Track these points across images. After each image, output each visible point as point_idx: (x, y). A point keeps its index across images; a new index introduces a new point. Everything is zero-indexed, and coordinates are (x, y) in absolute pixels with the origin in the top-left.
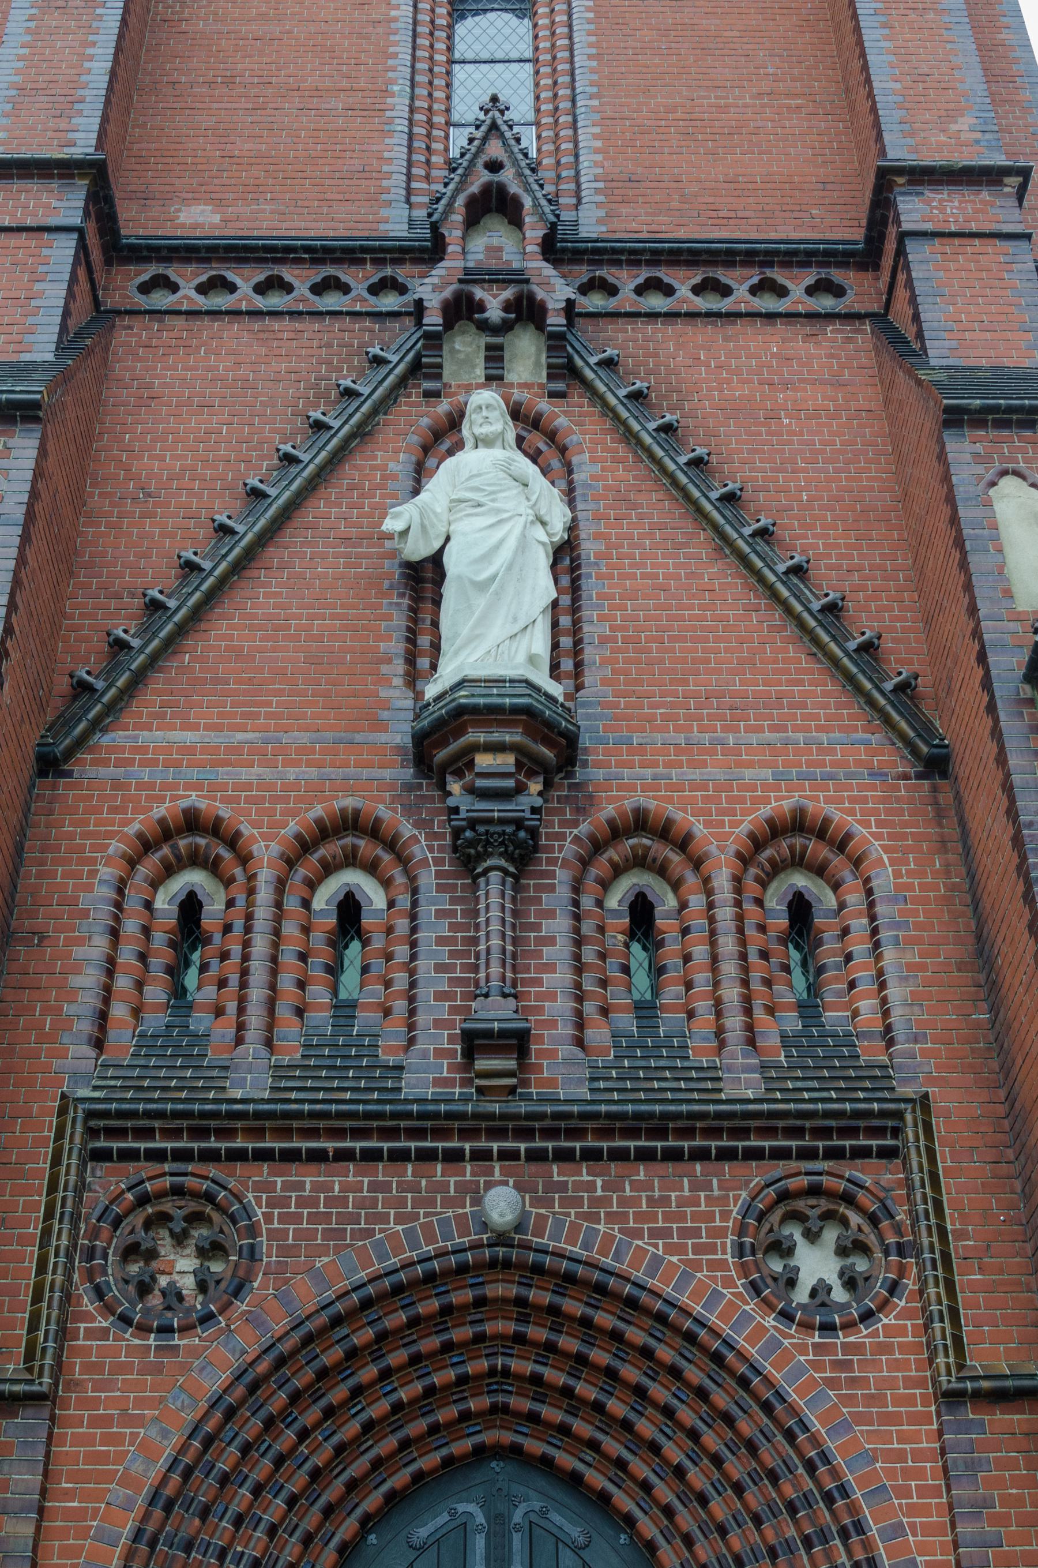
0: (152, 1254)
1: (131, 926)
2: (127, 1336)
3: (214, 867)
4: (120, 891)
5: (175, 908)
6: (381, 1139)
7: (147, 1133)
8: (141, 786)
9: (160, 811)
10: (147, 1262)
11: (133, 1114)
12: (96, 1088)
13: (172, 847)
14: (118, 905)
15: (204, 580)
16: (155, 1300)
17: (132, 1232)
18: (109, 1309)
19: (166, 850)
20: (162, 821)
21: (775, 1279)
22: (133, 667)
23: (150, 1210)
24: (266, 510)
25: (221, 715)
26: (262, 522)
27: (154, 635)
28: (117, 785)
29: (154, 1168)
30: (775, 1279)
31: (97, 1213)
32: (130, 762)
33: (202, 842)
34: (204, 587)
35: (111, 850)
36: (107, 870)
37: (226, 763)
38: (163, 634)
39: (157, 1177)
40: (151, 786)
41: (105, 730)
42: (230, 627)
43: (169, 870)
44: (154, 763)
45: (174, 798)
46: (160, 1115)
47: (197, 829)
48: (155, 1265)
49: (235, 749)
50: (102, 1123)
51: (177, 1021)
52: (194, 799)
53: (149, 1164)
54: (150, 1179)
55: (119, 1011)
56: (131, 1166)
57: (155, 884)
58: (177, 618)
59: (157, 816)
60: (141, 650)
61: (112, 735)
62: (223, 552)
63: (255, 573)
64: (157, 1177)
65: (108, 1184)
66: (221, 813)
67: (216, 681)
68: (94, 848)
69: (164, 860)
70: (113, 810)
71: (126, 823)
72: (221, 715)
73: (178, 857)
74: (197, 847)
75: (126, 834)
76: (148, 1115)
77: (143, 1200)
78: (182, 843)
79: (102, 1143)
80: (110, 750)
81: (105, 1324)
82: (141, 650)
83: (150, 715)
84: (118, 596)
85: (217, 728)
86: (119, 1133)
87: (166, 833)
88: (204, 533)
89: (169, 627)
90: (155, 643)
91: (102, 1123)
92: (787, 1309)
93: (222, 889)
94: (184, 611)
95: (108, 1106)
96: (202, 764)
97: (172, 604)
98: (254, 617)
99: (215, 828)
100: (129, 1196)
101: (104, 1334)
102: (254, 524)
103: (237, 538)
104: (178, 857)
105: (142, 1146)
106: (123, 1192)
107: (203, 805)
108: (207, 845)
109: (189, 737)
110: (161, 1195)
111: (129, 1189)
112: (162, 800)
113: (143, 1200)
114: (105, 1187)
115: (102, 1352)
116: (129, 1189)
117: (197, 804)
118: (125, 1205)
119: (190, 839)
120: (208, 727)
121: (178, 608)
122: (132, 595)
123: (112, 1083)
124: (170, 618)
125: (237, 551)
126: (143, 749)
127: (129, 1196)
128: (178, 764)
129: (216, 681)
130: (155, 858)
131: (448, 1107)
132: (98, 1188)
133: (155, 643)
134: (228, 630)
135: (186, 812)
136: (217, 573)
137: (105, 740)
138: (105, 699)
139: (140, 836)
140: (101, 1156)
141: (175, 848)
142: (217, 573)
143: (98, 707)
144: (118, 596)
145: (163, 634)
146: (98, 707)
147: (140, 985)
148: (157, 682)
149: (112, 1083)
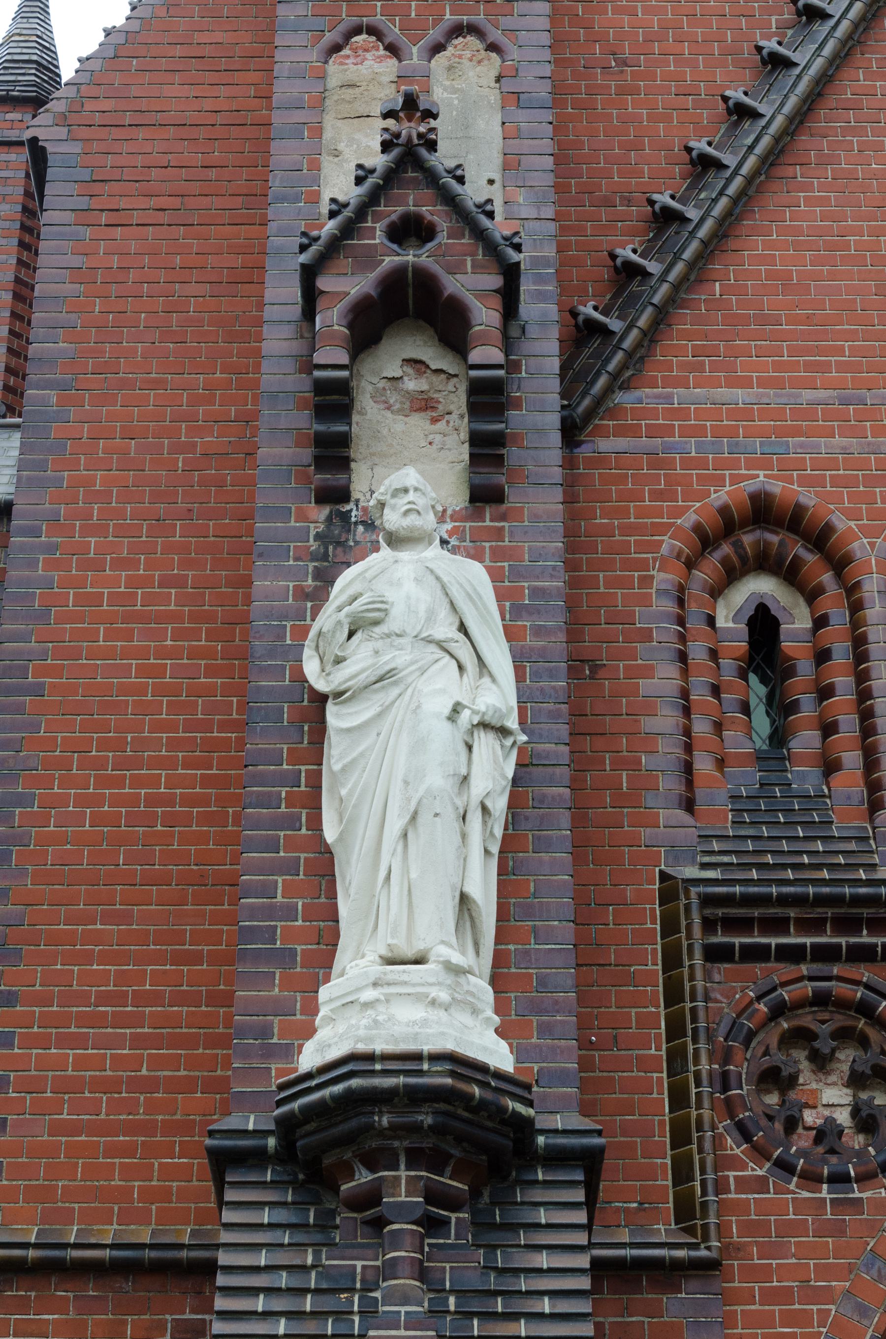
0: (792, 1081)
1: (698, 651)
2: (792, 1187)
3: (791, 574)
4: (681, 602)
5: (743, 627)
6: (764, 932)
7: (779, 925)
8: (688, 463)
9: (720, 496)
10: (783, 1092)
11: (764, 900)
12: (704, 866)
13: (734, 544)
14: (681, 621)
15: (729, 181)
16: (802, 1141)
17: (766, 1053)
18: (760, 1153)
19: (726, 549)
20: (724, 511)
21: (771, 1118)
22: (656, 300)
23: (786, 1025)
24: (795, 85)
25: (778, 366)
26: (792, 101)
27: (677, 257)
28: (656, 461)
29: (787, 970)
30: (771, 1118)
31: (723, 1029)
32: (668, 431)
33: (774, 539)
34: (731, 190)
35: (664, 549)
36: (663, 575)
37: (796, 432)
38: (687, 255)
39: (797, 983)
40: (702, 464)
41: (626, 386)
42: (767, 246)
43: (732, 575)
44: (700, 431)
45: (735, 479)
46: (799, 901)
47: (767, 522)
48: (792, 1095)
49: (805, 413)
50: (720, 912)
51: (773, 777)
52: (761, 480)
53: (782, 965)
54: (784, 984)
55: (703, 764)
56: (758, 968)
57: (716, 592)
58: (702, 233)
59: (718, 504)
60: (662, 279)
61: (638, 393)
62: (749, 141)
63: (789, 171)
64: (797, 983)
65: (726, 994)
66: (803, 500)
67: (763, 320)
68: (643, 547)
69: (725, 562)
70: (657, 495)
71: (679, 512)
72: (778, 366)
73: (743, 559)
74: (767, 544)
75: (679, 527)
76: (784, 901)
77: (779, 1010)
78: (747, 539)
79: (719, 938)
80: (640, 414)
81: (759, 1172)
82: (662, 279)
83: (682, 366)
84: (608, 203)
85: (776, 383)
86: (743, 925)
87: (729, 524)
88: (711, 114)
89: (694, 247)
90: (679, 267)
91: (720, 912)
92: (786, 1157)
93: (801, 601)
94: (709, 224)
95: (731, 889)
96: (763, 433)
97: (693, 213)
98: (798, 231)
99: (794, 520)
100: (762, 1007)
101: (761, 1184)
102: (782, 104)
103: (763, 122)
104: (743, 559)
105: (773, 941)
106: (751, 1003)
107: (776, 488)
108: (781, 543)
109: (740, 395)
110: (800, 1004)
111: (759, 998)
112: (719, 481)
113: (779, 1010)
114: (729, 995)
115: (763, 1207)
116: (759, 998)
117: (768, 488)
118: (758, 1018)
119: (758, 533)
120: (763, 383)
121: (702, 220)
122: (628, 202)
123: (726, 859)
124: (692, 233)
125: (766, 141)
126: (681, 413)
127: (762, 1007)
128: (732, 433)
129: (763, 320)
130: (714, 559)
131: (743, 889)
132: (719, 997)
133: (679, 267)
134: (766, 252)
135: (755, 497)
136: (744, 170)
137: (621, 398)
138: (627, 344)
139: (698, 529)
140: (716, 954)
141: (738, 546)
142: (744, 170)
143: (619, 356)
144: (608, 203)
145: (687, 255)
146: (619, 356)
147: (718, 727)
148: (684, 322)
149: (726, 859)
